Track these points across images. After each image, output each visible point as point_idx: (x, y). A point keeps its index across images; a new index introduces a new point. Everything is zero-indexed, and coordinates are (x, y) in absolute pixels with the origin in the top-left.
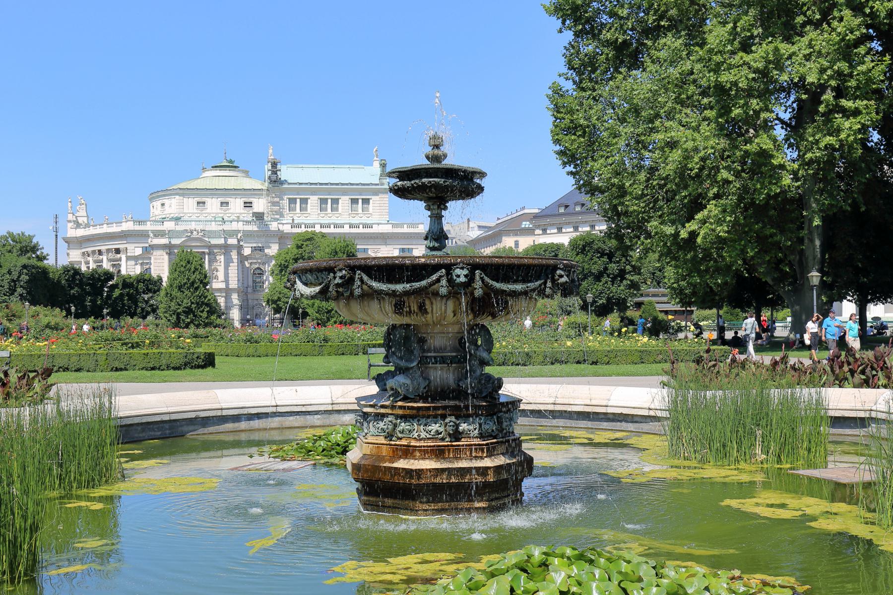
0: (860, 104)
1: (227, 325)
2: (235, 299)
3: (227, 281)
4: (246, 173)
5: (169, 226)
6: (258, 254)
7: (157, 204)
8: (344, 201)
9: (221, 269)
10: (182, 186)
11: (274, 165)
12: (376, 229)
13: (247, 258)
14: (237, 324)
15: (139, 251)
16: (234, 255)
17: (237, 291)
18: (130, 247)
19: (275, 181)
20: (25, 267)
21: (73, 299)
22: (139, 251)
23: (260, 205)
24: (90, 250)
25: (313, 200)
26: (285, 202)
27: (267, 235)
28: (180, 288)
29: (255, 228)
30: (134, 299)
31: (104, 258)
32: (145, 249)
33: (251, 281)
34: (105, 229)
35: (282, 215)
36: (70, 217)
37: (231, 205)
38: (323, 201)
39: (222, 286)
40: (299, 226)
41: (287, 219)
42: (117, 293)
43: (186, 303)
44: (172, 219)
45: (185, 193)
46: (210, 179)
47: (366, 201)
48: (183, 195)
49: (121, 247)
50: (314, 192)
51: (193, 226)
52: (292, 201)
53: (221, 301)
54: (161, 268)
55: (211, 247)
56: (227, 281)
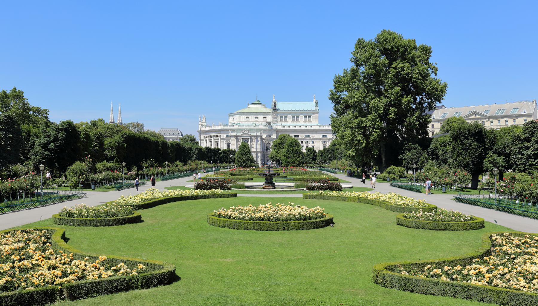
0: (377, 130)
1: (256, 166)
2: (259, 154)
3: (257, 149)
4: (265, 106)
5: (236, 127)
6: (268, 138)
7: (231, 118)
8: (301, 117)
9: (255, 144)
10: (240, 111)
11: (275, 103)
12: (313, 128)
13: (264, 139)
14: (260, 166)
15: (225, 137)
16: (259, 139)
17: (261, 152)
18: (222, 135)
19: (275, 109)
20: (196, 149)
21: (208, 157)
22: (225, 137)
23: (269, 119)
24: (207, 135)
25: (290, 116)
26: (279, 117)
27: (272, 130)
28: (242, 154)
29: (267, 128)
30: (227, 157)
31: (213, 139)
32: (227, 136)
33: (265, 149)
34: (213, 128)
35: (277, 122)
36: (200, 123)
37: (259, 119)
38: (293, 117)
39: (255, 150)
40: (284, 127)
41: (279, 124)
42: (221, 155)
43: (244, 159)
44: (237, 124)
45: (241, 114)
46: (252, 108)
47: (310, 117)
48: (241, 115)
49: (218, 135)
50: (290, 114)
51: (245, 127)
52: (281, 117)
53: (254, 156)
54: (234, 147)
55: (251, 136)
56: (257, 149)
